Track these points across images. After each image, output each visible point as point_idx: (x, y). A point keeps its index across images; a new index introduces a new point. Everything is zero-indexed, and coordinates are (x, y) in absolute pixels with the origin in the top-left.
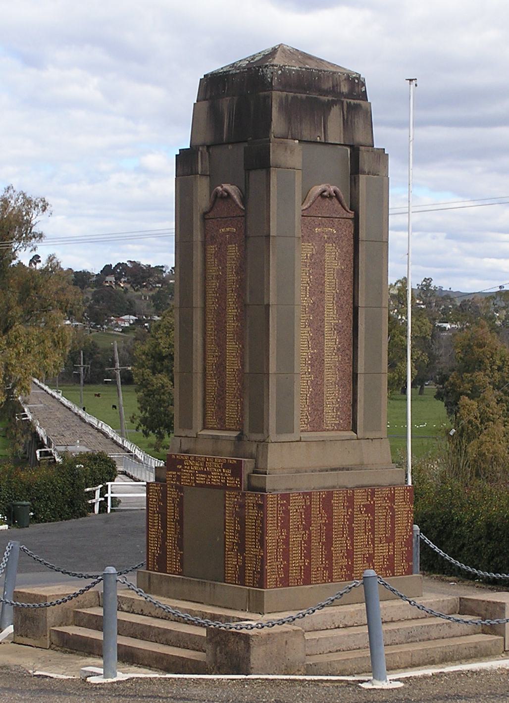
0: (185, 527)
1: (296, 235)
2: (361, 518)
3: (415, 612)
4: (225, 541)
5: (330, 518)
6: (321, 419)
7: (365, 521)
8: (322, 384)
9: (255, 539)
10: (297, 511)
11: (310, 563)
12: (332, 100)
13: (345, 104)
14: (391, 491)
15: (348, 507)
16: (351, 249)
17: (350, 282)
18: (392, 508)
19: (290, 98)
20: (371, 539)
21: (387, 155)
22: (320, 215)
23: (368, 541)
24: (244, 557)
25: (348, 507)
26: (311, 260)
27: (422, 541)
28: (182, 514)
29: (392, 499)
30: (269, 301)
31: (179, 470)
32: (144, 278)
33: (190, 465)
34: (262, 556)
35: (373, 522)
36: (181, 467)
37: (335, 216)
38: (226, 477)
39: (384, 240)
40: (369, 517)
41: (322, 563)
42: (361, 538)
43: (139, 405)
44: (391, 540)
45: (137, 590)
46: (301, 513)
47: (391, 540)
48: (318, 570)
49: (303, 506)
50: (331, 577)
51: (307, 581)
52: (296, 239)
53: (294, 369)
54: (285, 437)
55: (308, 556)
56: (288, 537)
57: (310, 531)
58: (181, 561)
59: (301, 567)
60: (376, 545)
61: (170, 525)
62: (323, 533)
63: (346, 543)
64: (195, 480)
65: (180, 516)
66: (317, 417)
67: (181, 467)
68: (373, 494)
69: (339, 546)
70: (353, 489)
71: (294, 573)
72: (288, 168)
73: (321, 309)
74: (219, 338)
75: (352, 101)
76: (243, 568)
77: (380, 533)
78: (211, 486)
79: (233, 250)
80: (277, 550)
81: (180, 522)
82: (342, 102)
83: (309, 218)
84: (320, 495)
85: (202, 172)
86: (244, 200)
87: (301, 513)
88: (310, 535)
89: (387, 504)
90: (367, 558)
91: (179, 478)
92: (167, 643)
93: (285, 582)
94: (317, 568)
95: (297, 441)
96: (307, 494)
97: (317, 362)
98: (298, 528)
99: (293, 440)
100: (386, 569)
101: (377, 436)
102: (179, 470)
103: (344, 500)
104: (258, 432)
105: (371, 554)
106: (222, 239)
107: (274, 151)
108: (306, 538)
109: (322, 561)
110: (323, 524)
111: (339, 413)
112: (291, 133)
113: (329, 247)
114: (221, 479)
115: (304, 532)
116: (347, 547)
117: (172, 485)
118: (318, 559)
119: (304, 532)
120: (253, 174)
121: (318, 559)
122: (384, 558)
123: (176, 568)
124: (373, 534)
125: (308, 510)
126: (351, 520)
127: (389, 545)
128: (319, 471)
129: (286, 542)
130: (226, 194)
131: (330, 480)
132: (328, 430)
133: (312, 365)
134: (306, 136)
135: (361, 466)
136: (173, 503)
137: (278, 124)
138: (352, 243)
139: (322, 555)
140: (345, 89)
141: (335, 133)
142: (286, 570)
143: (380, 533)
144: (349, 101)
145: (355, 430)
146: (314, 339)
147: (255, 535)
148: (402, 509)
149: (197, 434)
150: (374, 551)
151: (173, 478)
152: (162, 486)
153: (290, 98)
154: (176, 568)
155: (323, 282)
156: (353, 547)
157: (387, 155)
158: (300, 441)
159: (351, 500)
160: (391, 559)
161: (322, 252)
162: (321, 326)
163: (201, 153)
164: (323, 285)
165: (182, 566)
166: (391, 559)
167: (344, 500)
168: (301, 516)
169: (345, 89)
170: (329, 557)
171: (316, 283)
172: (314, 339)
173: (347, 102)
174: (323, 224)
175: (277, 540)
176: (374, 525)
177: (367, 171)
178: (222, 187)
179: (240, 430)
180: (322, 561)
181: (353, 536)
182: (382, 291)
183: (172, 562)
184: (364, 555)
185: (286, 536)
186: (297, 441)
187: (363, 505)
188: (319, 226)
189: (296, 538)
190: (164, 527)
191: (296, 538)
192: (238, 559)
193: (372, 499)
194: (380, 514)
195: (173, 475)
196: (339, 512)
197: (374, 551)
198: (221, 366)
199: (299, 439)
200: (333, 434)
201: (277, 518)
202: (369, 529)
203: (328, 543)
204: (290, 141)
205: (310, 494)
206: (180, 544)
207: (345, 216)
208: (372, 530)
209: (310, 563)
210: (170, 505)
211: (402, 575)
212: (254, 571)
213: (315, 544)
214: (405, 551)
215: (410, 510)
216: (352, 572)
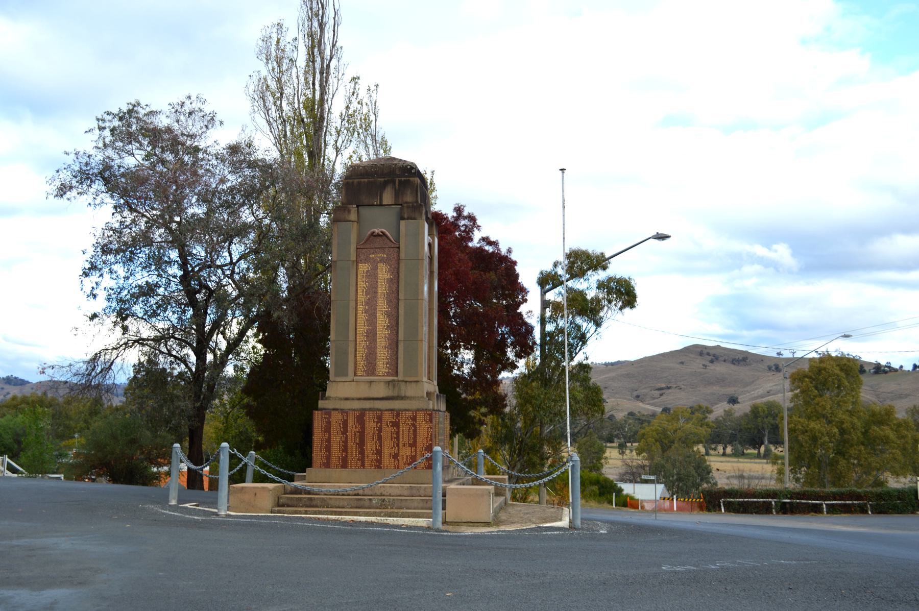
1: (352, 259)
8: (375, 348)
11: (346, 456)
15: (377, 422)
18: (414, 425)
25: (377, 422)
32: (581, 310)
35: (398, 433)
39: (420, 258)
42: (387, 444)
46: (340, 424)
47: (414, 445)
50: (363, 465)
51: (344, 466)
54: (338, 379)
56: (329, 438)
57: (346, 435)
68: (398, 415)
69: (370, 446)
71: (334, 461)
73: (375, 303)
77: (404, 438)
87: (340, 424)
88: (346, 438)
89: (410, 422)
92: (354, 512)
93: (327, 465)
97: (371, 335)
108: (343, 439)
113: (381, 265)
118: (353, 452)
124: (398, 441)
125: (345, 423)
126: (380, 430)
129: (329, 441)
132: (380, 376)
133: (367, 336)
142: (328, 458)
145: (397, 376)
158: (353, 381)
159: (380, 419)
161: (375, 268)
164: (376, 288)
170: (362, 452)
177: (406, 216)
188: (373, 253)
189: (336, 439)
191: (336, 439)
193: (397, 418)
194: (403, 428)
196: (370, 425)
202: (395, 438)
203: (361, 444)
208: (398, 438)
213: (351, 444)
216: (381, 463)
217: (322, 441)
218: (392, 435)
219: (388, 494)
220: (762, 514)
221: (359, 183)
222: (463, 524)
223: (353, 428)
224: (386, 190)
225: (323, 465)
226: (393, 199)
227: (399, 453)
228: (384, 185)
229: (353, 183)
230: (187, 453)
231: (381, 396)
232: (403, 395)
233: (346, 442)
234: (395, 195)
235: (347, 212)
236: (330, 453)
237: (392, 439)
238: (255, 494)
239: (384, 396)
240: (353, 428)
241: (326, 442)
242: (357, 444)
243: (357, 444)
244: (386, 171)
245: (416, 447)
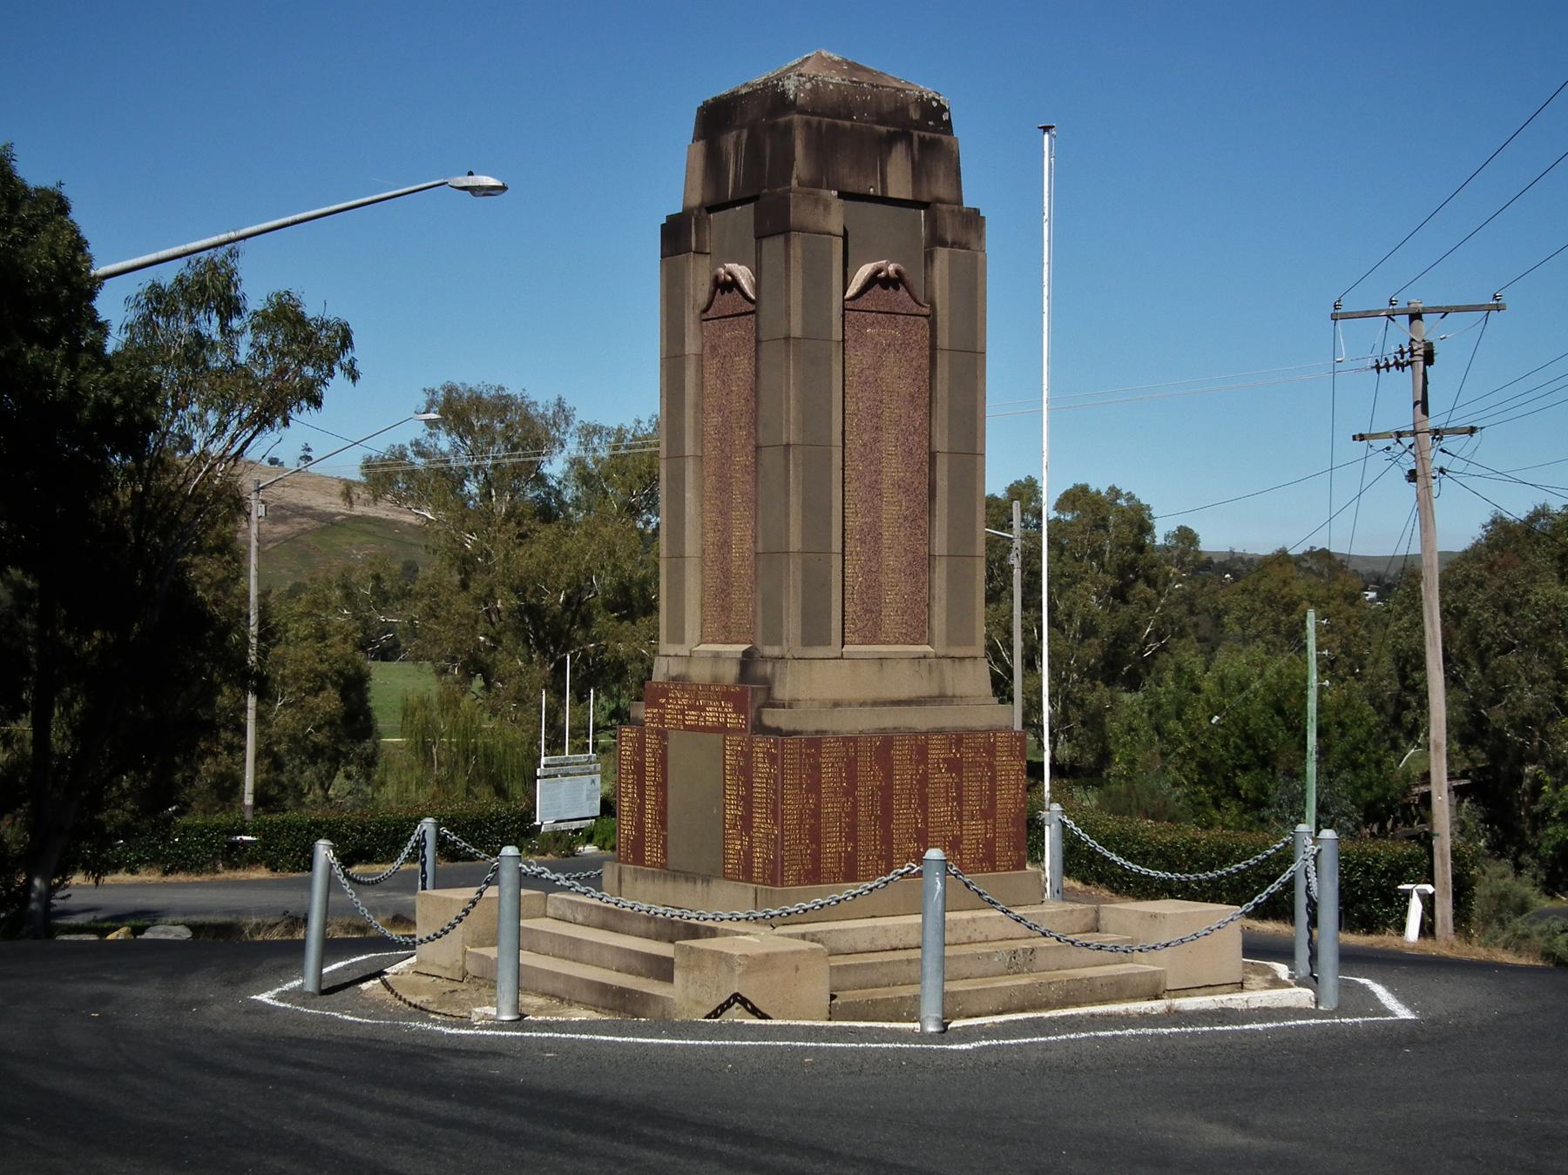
0: (670, 792)
2: (940, 778)
3: (1020, 929)
4: (725, 814)
5: (889, 776)
6: (878, 626)
7: (947, 783)
9: (767, 808)
10: (832, 766)
11: (855, 848)
12: (895, 132)
13: (915, 139)
14: (989, 737)
15: (918, 762)
16: (925, 362)
17: (925, 413)
19: (824, 127)
20: (957, 812)
21: (984, 217)
22: (874, 309)
23: (952, 816)
24: (751, 838)
25: (918, 762)
26: (860, 377)
27: (1064, 825)
28: (666, 775)
29: (991, 750)
30: (788, 438)
31: (662, 706)
33: (676, 698)
34: (776, 836)
35: (959, 787)
36: (664, 701)
37: (899, 311)
38: (726, 714)
40: (953, 779)
41: (876, 849)
43: (268, 429)
44: (988, 814)
45: (583, 890)
46: (841, 769)
48: (869, 860)
49: (843, 758)
52: (834, 344)
53: (831, 546)
55: (852, 836)
56: (818, 805)
57: (855, 797)
58: (664, 847)
59: (840, 854)
60: (965, 823)
61: (650, 792)
62: (877, 802)
63: (915, 817)
64: (684, 720)
65: (662, 777)
66: (871, 623)
67: (664, 701)
70: (926, 733)
71: (828, 863)
72: (820, 234)
74: (722, 502)
75: (927, 135)
76: (749, 855)
77: (972, 805)
78: (705, 729)
79: (743, 364)
80: (800, 828)
81: (662, 786)
82: (911, 135)
83: (856, 313)
84: (871, 741)
85: (696, 248)
86: (757, 287)
87: (841, 769)
88: (855, 805)
90: (949, 842)
91: (662, 719)
94: (868, 856)
95: (836, 658)
96: (850, 739)
98: (835, 793)
99: (831, 656)
100: (981, 861)
101: (969, 654)
102: (662, 706)
103: (912, 751)
104: (772, 644)
105: (957, 836)
106: (727, 349)
107: (796, 206)
108: (848, 807)
109: (875, 846)
110: (877, 787)
111: (905, 618)
112: (827, 179)
114: (718, 717)
115: (844, 799)
116: (917, 823)
117: (652, 729)
119: (844, 799)
120: (767, 244)
121: (868, 833)
122: (978, 843)
123: (657, 857)
124: (960, 804)
125: (851, 765)
126: (924, 781)
127: (986, 823)
128: (1310, 941)
129: (816, 814)
130: (729, 278)
131: (889, 719)
134: (852, 185)
135: (941, 699)
136: (653, 757)
137: (801, 167)
138: (928, 353)
139: (875, 835)
140: (915, 115)
141: (899, 184)
142: (816, 858)
143: (972, 805)
144: (922, 133)
146: (866, 501)
147: (767, 803)
148: (1009, 768)
149: (691, 651)
150: (961, 832)
151: (653, 718)
152: (638, 731)
153: (824, 127)
154: (657, 857)
155: (879, 412)
156: (926, 825)
157: (984, 217)
159: (922, 752)
160: (989, 844)
162: (876, 482)
163: (696, 219)
165: (665, 855)
166: (989, 844)
167: (912, 751)
168: (841, 774)
169: (915, 115)
171: (868, 414)
172: (866, 501)
173: (919, 136)
174: (879, 323)
175: (801, 811)
176: (962, 791)
177: (949, 238)
178: (724, 267)
179: (751, 643)
180: (875, 846)
181: (928, 808)
182: (976, 428)
183: (651, 853)
184: (945, 837)
185: (815, 805)
186: (836, 658)
187: (943, 759)
188: (872, 325)
190: (642, 795)
192: (742, 840)
193: (958, 750)
195: (654, 713)
196: (903, 776)
197: (961, 832)
198: (724, 545)
199: (839, 655)
200: (898, 648)
201: (801, 777)
204: (824, 193)
205: (854, 740)
206: (662, 820)
207: (915, 311)
208: (959, 799)
209: (855, 848)
210: (649, 758)
211: (1009, 870)
212: (765, 859)
214: (1014, 833)
215: (1022, 770)
217: (801, 815)
218: (947, 792)
219: (982, 938)
220: (1340, 899)
221: (833, 127)
222: (1196, 991)
223: (868, 778)
224: (894, 153)
225: (806, 877)
226: (910, 189)
227: (962, 835)
228: (889, 141)
229: (820, 123)
230: (1106, 893)
231: (904, 693)
232: (950, 694)
233: (853, 813)
234: (913, 168)
235: (821, 207)
236: (819, 845)
237: (947, 801)
238: (797, 969)
239: (913, 695)
240: (868, 778)
241: (811, 816)
242: (877, 817)
243: (877, 817)
244: (886, 108)
245: (995, 819)
